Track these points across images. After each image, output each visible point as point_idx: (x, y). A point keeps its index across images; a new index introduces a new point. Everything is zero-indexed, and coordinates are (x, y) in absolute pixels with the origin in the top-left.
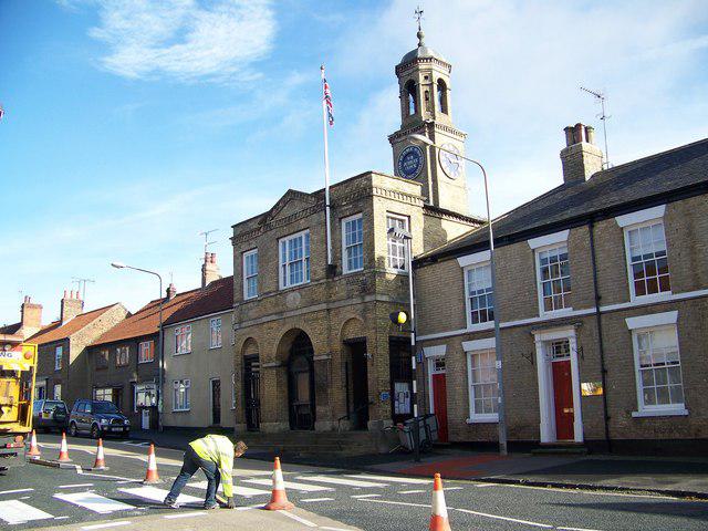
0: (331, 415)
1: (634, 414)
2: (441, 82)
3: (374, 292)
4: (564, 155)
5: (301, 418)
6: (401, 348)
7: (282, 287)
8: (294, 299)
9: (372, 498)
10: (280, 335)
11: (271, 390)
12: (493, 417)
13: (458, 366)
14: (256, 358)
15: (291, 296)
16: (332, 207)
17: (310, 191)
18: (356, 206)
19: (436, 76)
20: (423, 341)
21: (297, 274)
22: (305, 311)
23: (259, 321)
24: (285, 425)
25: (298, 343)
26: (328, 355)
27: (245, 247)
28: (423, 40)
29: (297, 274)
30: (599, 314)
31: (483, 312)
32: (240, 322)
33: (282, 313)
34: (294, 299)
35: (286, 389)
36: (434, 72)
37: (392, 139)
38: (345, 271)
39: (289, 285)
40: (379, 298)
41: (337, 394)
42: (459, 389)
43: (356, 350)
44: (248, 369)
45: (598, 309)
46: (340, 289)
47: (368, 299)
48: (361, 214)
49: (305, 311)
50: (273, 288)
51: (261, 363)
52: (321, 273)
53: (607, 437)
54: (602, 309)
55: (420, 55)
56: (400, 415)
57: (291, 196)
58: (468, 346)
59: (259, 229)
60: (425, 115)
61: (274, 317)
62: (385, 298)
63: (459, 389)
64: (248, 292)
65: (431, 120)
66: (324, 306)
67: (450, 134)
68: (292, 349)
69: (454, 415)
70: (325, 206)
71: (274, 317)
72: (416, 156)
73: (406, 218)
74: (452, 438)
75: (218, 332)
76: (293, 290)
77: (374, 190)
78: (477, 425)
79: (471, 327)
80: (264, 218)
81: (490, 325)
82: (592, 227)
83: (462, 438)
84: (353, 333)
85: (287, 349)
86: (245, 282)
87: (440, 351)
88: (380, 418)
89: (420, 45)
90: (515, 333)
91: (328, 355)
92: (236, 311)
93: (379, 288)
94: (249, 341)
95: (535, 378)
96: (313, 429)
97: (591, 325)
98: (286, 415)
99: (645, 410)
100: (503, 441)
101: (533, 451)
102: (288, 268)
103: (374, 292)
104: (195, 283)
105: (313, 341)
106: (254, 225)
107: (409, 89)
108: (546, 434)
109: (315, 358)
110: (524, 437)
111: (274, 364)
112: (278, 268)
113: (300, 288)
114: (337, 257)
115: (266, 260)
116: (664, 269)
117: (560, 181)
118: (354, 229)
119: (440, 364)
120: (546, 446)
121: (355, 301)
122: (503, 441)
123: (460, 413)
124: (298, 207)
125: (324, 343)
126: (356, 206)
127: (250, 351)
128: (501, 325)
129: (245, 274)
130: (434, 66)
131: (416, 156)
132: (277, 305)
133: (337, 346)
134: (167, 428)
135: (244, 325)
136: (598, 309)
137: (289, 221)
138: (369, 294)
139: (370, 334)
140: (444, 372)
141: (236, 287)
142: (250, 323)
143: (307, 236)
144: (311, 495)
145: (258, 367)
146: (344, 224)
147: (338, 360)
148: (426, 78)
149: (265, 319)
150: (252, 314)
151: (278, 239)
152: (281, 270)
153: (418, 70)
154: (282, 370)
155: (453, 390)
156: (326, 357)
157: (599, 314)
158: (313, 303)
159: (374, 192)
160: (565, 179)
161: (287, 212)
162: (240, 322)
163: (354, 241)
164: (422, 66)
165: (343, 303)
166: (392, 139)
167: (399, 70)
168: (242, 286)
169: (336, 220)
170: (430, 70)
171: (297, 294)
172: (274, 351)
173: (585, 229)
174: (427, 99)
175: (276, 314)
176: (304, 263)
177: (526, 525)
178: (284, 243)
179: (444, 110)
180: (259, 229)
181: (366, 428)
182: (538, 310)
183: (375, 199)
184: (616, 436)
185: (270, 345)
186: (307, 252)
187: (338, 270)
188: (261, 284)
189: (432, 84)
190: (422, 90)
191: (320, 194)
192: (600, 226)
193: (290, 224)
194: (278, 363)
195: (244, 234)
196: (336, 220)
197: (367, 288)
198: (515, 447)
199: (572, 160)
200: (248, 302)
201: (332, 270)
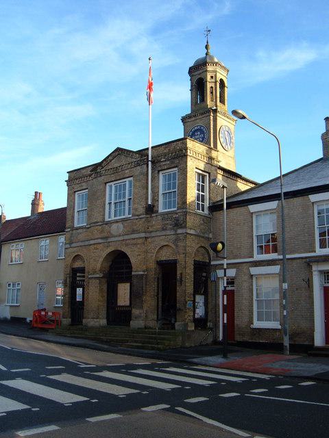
0: (145, 316)
2: (222, 82)
3: (185, 227)
5: (119, 316)
6: (203, 271)
7: (107, 219)
8: (117, 229)
10: (104, 254)
11: (93, 295)
12: (275, 325)
13: (246, 285)
14: (82, 270)
15: (114, 226)
17: (135, 150)
19: (219, 77)
20: (217, 265)
21: (120, 210)
22: (126, 237)
23: (87, 243)
24: (103, 322)
26: (144, 271)
29: (120, 210)
32: (71, 243)
33: (106, 238)
34: (117, 229)
35: (105, 294)
36: (218, 74)
37: (184, 120)
38: (161, 210)
39: (113, 218)
40: (189, 231)
41: (150, 301)
42: (245, 302)
43: (168, 270)
44: (75, 278)
46: (156, 222)
47: (180, 231)
48: (176, 169)
49: (126, 237)
50: (100, 219)
51: (86, 274)
52: (141, 210)
55: (208, 61)
57: (119, 152)
58: (254, 270)
59: (90, 175)
60: (209, 103)
61: (100, 241)
62: (192, 232)
63: (245, 302)
64: (79, 221)
65: (215, 108)
66: (143, 235)
67: (228, 120)
68: (112, 264)
69: (240, 321)
70: (148, 161)
71: (100, 241)
72: (202, 132)
73: (208, 175)
74: (238, 338)
75: (49, 247)
76: (117, 222)
77: (189, 151)
78: (260, 330)
79: (257, 257)
80: (95, 168)
83: (246, 338)
84: (166, 256)
85: (107, 265)
86: (76, 214)
87: (232, 273)
88: (184, 322)
89: (207, 54)
91: (144, 271)
92: (68, 235)
93: (189, 224)
94: (77, 257)
95: (311, 298)
96: (129, 326)
98: (103, 312)
100: (286, 342)
101: (309, 352)
103: (185, 227)
104: (26, 212)
105: (133, 260)
107: (199, 87)
109: (133, 273)
110: (301, 341)
111: (98, 276)
112: (105, 205)
113: (123, 220)
114: (155, 199)
115: (95, 199)
118: (169, 180)
119: (231, 282)
120: (319, 349)
121: (168, 232)
122: (286, 342)
123: (246, 320)
124: (124, 160)
125: (142, 261)
127: (78, 264)
128: (288, 256)
129: (76, 207)
130: (218, 69)
131: (202, 132)
132: (102, 232)
133: (153, 265)
135: (73, 245)
137: (116, 170)
138: (181, 228)
139: (180, 258)
140: (233, 288)
141: (69, 217)
143: (130, 182)
144: (59, 372)
145: (84, 277)
146: (76, 196)
147: (152, 275)
148: (212, 77)
149: (92, 242)
150: (81, 237)
151: (106, 183)
152: (107, 206)
153: (206, 71)
154: (104, 281)
155: (241, 302)
156: (142, 273)
158: (133, 232)
159: (189, 153)
160: (324, 155)
162: (71, 243)
163: (120, 198)
164: (210, 68)
165: (158, 233)
166: (184, 120)
168: (73, 217)
169: (156, 171)
170: (216, 72)
171: (120, 225)
172: (99, 266)
174: (212, 93)
175: (101, 238)
176: (127, 203)
177: (321, 402)
178: (111, 186)
179: (222, 101)
180: (90, 175)
181: (173, 327)
182: (314, 247)
183: (189, 158)
185: (96, 260)
186: (130, 195)
187: (155, 209)
188: (89, 217)
189: (216, 82)
190: (209, 85)
191: (143, 153)
193: (118, 174)
195: (76, 179)
196: (156, 171)
197: (179, 223)
198: (295, 349)
199: (35, 204)
200: (77, 229)
201: (151, 209)
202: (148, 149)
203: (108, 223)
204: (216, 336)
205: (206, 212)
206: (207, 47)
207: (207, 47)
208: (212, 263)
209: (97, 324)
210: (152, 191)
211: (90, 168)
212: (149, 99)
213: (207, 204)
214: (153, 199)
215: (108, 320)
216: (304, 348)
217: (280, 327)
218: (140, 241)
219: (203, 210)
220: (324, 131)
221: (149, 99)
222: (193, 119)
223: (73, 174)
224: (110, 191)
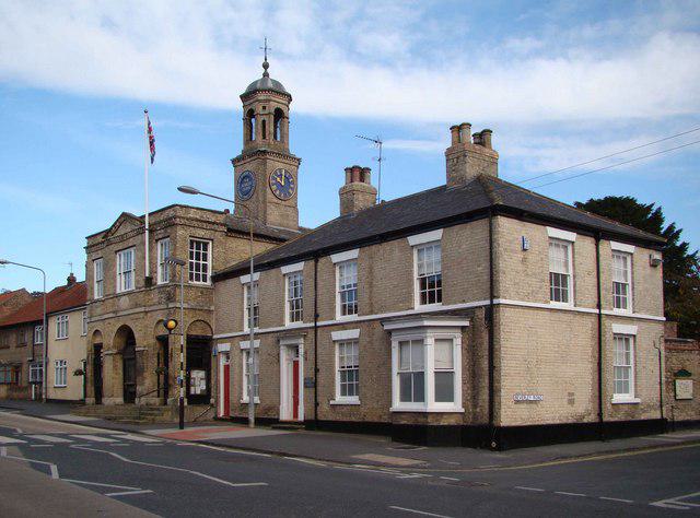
1: (332, 402)
4: (343, 192)
7: (118, 291)
9: (127, 490)
11: (112, 374)
16: (151, 231)
18: (166, 232)
25: (126, 334)
27: (94, 256)
28: (268, 70)
30: (316, 327)
31: (350, 306)
37: (234, 161)
38: (160, 282)
39: (123, 290)
45: (492, 302)
47: (171, 305)
50: (111, 292)
52: (142, 283)
53: (600, 415)
54: (318, 324)
56: (196, 396)
61: (111, 315)
80: (107, 233)
81: (354, 317)
82: (317, 262)
90: (270, 337)
97: (311, 335)
98: (121, 392)
99: (339, 399)
102: (123, 276)
104: (438, 179)
105: (136, 336)
106: (100, 239)
108: (285, 414)
110: (272, 415)
113: (129, 293)
115: (108, 267)
116: (439, 284)
117: (337, 214)
119: (227, 354)
125: (145, 340)
126: (166, 232)
133: (153, 341)
134: (49, 401)
136: (492, 302)
137: (122, 239)
142: (97, 318)
148: (264, 108)
149: (106, 316)
150: (99, 311)
152: (118, 277)
157: (316, 327)
158: (137, 306)
161: (122, 231)
166: (234, 161)
167: (244, 97)
168: (92, 288)
169: (154, 241)
171: (126, 298)
173: (312, 263)
184: (321, 417)
185: (109, 339)
192: (322, 261)
194: (115, 351)
196: (154, 241)
198: (260, 422)
201: (149, 281)
202: (144, 216)
203: (118, 296)
204: (217, 413)
205: (209, 283)
206: (266, 66)
207: (266, 66)
208: (215, 337)
209: (112, 403)
210: (150, 263)
211: (102, 235)
212: (152, 159)
213: (209, 274)
214: (151, 272)
215: (125, 400)
216: (268, 420)
217: (463, 410)
218: (142, 315)
219: (205, 280)
220: (450, 145)
221: (152, 159)
222: (242, 162)
223: (92, 242)
224: (120, 263)
